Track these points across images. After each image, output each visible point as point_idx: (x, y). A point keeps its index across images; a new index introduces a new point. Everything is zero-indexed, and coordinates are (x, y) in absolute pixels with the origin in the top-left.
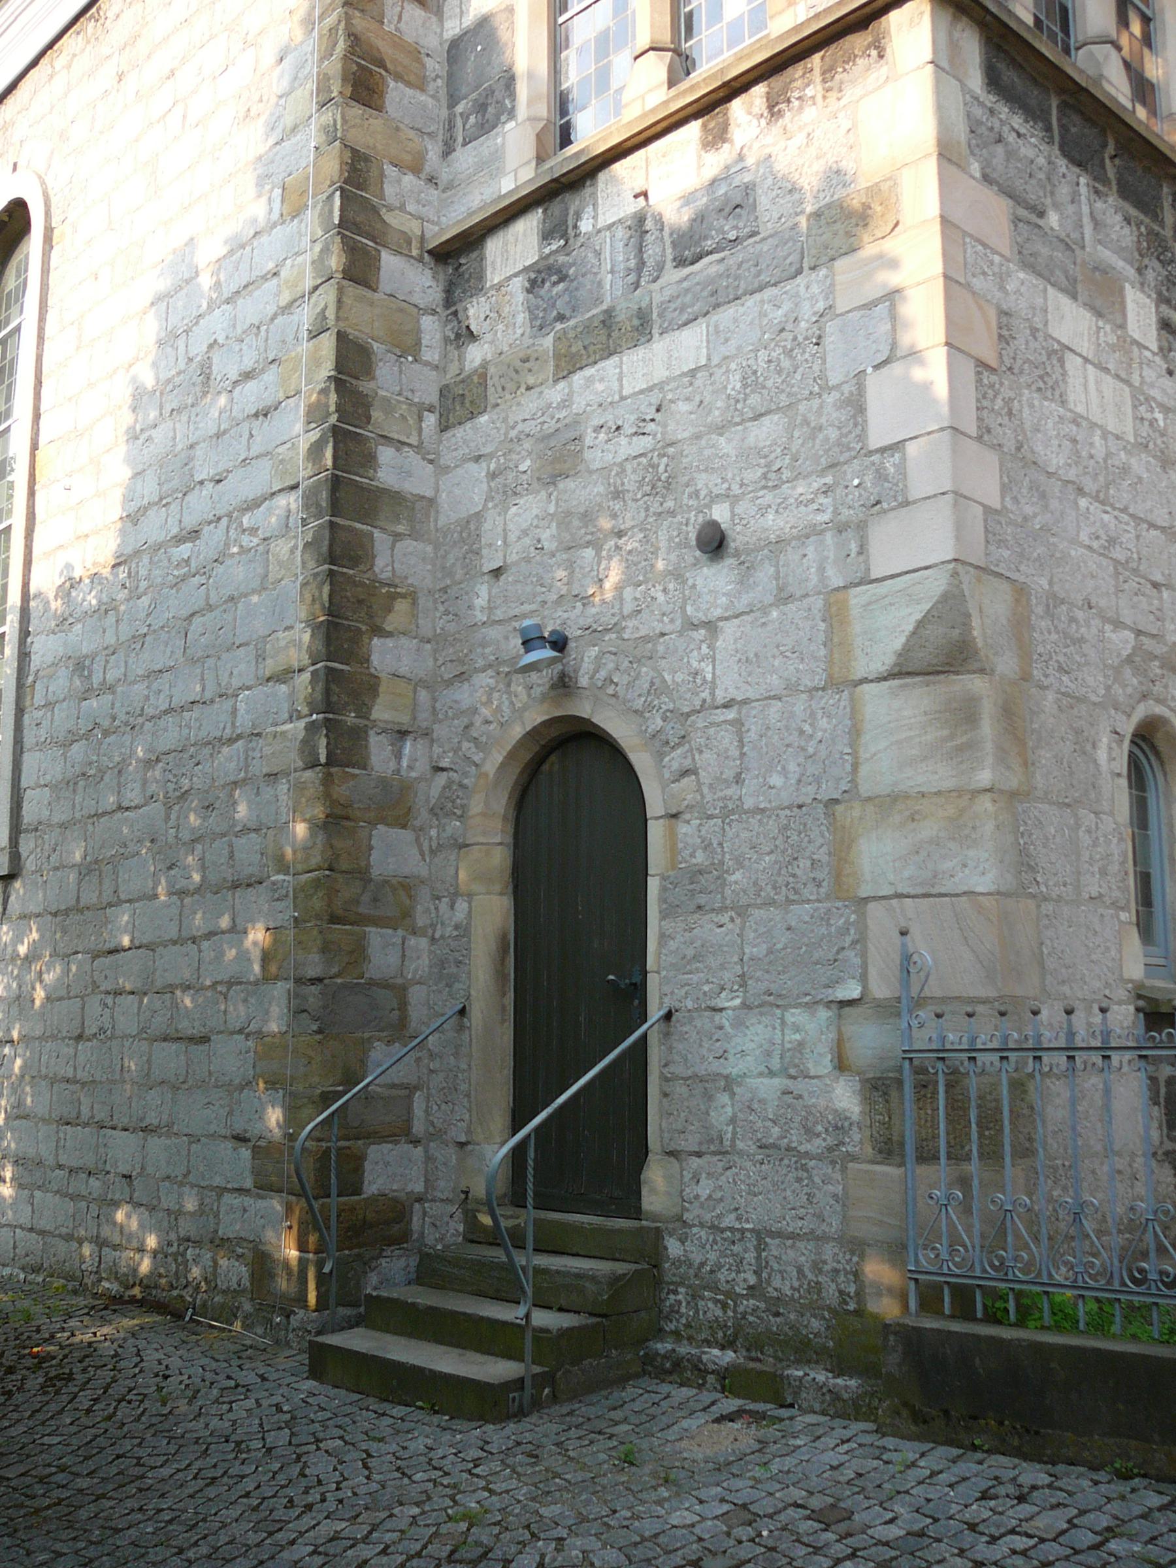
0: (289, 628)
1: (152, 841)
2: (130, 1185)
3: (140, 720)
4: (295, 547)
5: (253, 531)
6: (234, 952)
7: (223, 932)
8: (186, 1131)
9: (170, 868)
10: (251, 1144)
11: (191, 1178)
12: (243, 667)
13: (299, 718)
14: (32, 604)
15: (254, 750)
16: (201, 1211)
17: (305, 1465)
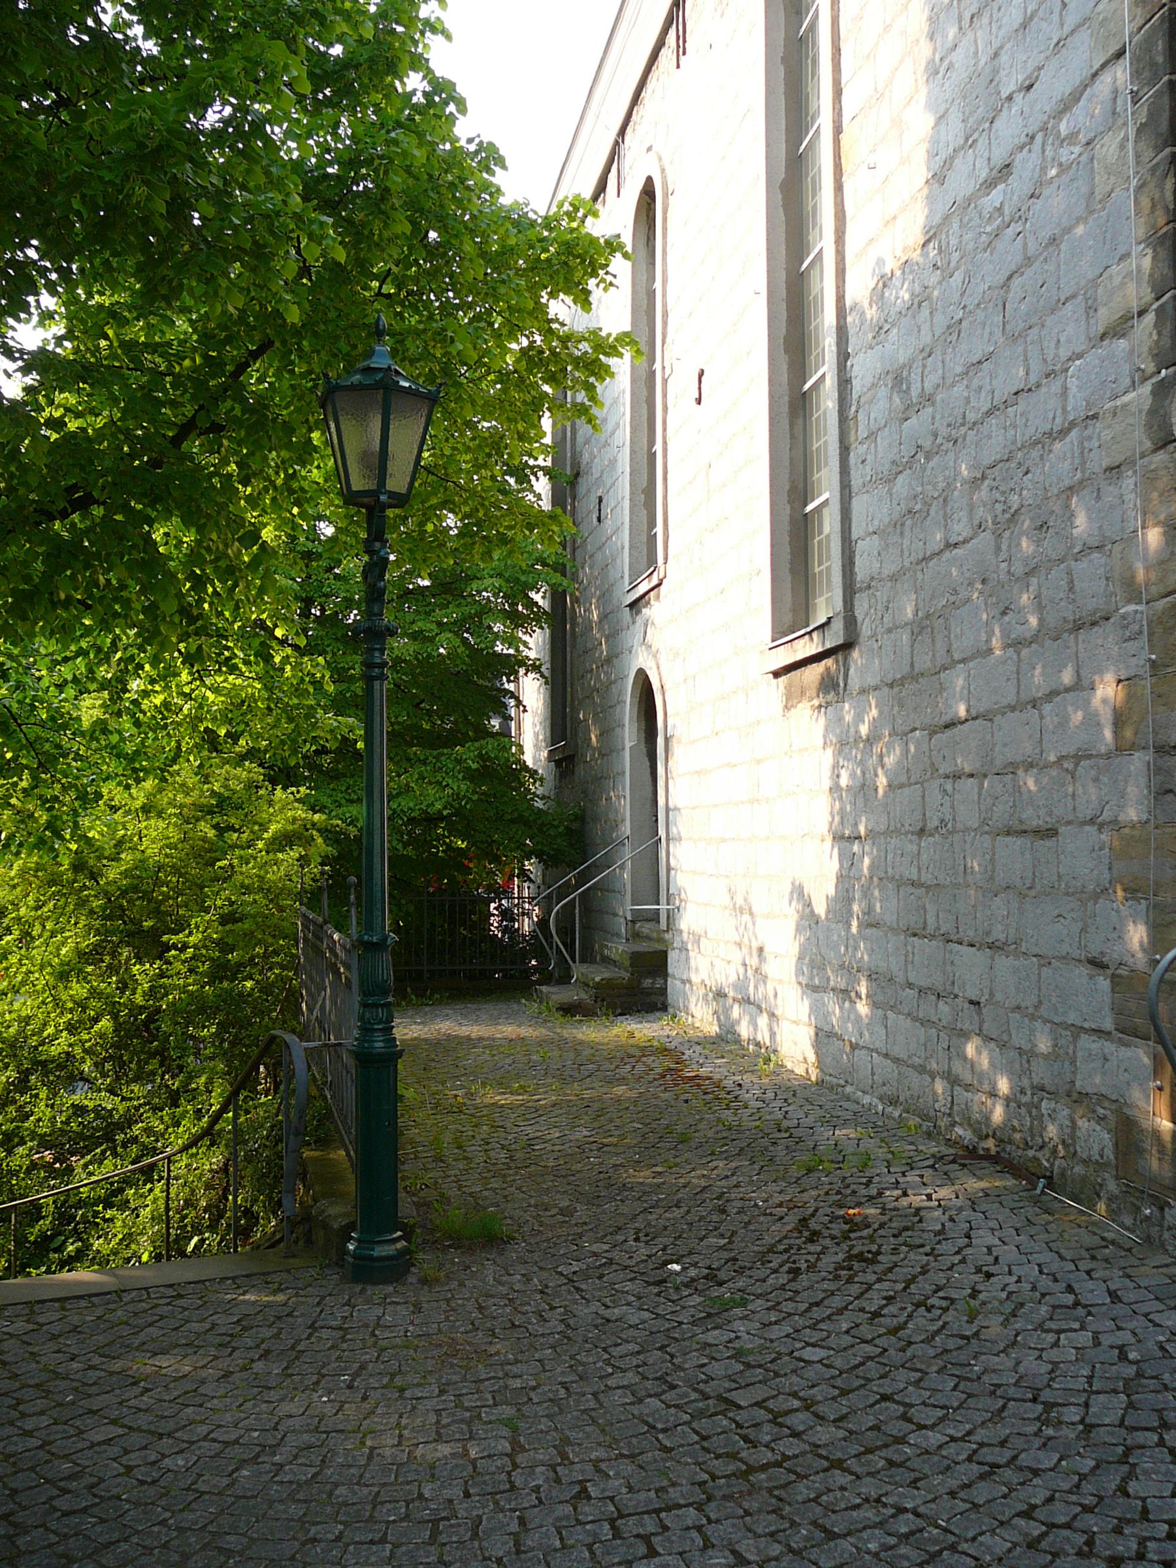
0: (1123, 258)
1: (984, 582)
2: (979, 1013)
3: (963, 430)
4: (1126, 138)
5: (1072, 138)
6: (1079, 715)
7: (1067, 690)
8: (1036, 950)
9: (1004, 613)
10: (1109, 972)
11: (1043, 1011)
12: (1070, 329)
13: (1145, 379)
14: (849, 319)
15: (1090, 438)
16: (1054, 1056)
17: (1131, 1475)
